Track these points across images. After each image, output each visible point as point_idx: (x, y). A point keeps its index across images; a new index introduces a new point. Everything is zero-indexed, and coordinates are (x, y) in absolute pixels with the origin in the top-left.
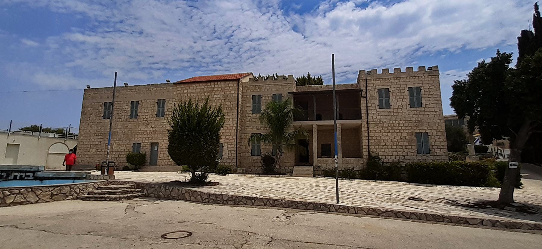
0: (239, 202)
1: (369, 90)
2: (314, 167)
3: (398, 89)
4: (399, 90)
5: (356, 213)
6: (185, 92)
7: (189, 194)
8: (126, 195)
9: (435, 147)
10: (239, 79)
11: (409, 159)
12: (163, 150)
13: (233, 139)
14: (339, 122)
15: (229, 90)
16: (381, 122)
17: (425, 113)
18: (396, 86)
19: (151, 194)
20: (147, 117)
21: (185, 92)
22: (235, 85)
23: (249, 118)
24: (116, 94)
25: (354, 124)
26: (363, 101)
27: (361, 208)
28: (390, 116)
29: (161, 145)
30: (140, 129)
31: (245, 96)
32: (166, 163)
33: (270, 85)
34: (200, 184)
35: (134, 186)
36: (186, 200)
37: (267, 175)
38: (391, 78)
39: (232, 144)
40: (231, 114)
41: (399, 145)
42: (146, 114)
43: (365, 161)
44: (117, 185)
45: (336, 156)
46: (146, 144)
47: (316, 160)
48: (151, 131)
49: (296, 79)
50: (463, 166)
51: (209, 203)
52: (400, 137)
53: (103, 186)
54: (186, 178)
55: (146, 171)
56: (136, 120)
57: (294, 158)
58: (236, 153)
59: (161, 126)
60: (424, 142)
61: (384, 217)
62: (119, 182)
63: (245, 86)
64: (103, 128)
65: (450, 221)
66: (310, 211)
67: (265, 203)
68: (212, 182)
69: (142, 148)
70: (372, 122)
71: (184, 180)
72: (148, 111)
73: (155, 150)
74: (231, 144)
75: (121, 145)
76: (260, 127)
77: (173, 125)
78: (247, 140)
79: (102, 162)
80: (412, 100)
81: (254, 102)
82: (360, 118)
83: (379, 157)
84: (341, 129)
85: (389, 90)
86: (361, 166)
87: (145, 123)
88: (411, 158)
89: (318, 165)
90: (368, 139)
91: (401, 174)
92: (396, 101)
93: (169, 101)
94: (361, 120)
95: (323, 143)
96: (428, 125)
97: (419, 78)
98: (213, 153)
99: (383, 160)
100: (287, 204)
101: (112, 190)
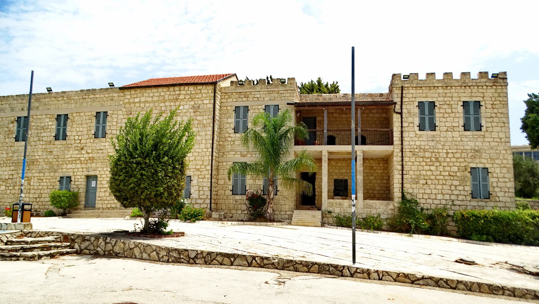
0: (212, 261)
1: (406, 103)
2: (322, 212)
3: (448, 103)
4: (449, 105)
5: (379, 279)
6: (137, 100)
7: (140, 249)
8: (48, 252)
9: (497, 189)
10: (217, 82)
11: (459, 206)
12: (104, 186)
13: (207, 170)
14: (360, 149)
15: (202, 99)
16: (422, 151)
17: (486, 140)
18: (446, 99)
19: (85, 250)
20: (80, 138)
21: (137, 100)
22: (210, 91)
23: (229, 139)
24: (34, 104)
25: (381, 151)
26: (396, 118)
27: (387, 272)
28: (435, 142)
29: (101, 179)
30: (70, 156)
31: (225, 108)
32: (109, 206)
33: (261, 93)
34: (156, 235)
35: (60, 238)
36: (136, 258)
37: (254, 223)
38: (438, 87)
39: (205, 177)
40: (203, 134)
41: (446, 184)
42: (80, 133)
43: (397, 205)
44: (35, 237)
45: (353, 196)
46: (79, 177)
47: (326, 202)
48: (87, 159)
49: (300, 86)
50: (535, 218)
51: (168, 262)
52: (447, 173)
53: (14, 240)
54: (136, 226)
55: (79, 217)
56: (64, 142)
57: (294, 198)
58: (211, 190)
59: (101, 151)
60: (482, 182)
61: (419, 286)
62: (38, 233)
63: (225, 92)
64: (16, 155)
65: (513, 295)
66: (314, 274)
67: (250, 262)
68: (174, 233)
69: (72, 183)
70: (408, 150)
71: (134, 230)
72: (81, 129)
73: (92, 186)
74: (203, 176)
75: (42, 180)
76: (245, 153)
77: (117, 148)
78: (226, 172)
79: (14, 205)
80: (467, 120)
81: (237, 116)
82: (392, 143)
83: (416, 201)
84: (363, 159)
85: (434, 104)
86: (390, 212)
87: (77, 147)
88: (463, 204)
89: (329, 210)
90: (402, 174)
91: (448, 227)
92: (445, 120)
93: (113, 114)
94: (392, 146)
95: (336, 177)
96: (488, 157)
97: (478, 88)
98: (176, 189)
99: (422, 205)
100: (281, 264)
101: (27, 244)
